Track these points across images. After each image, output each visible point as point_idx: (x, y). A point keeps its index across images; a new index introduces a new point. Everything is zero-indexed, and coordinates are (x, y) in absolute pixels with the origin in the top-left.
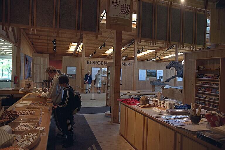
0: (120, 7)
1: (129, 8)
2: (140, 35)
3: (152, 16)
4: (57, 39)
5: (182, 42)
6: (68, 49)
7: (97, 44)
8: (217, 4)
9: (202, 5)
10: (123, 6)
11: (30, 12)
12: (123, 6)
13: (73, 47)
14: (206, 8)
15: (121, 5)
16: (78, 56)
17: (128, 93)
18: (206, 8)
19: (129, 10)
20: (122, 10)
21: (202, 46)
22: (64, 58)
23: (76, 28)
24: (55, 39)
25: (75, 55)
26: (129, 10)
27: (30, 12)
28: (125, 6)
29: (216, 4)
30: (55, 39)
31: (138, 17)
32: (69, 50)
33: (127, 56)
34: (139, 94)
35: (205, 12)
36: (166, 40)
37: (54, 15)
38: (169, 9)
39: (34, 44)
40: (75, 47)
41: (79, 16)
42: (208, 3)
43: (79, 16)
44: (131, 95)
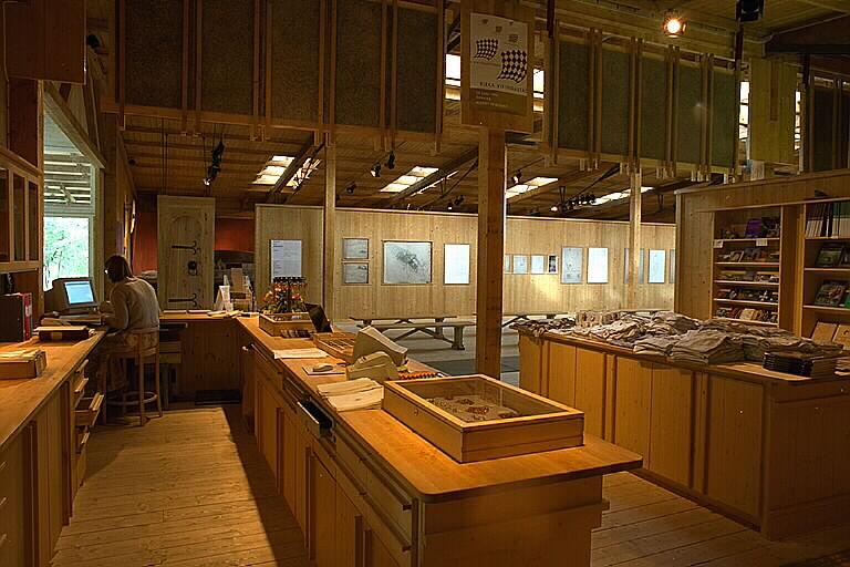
0: (498, 58)
1: (524, 62)
2: (555, 140)
3: (589, 84)
4: (227, 143)
5: (672, 160)
6: (256, 178)
7: (363, 160)
8: (766, 44)
9: (725, 48)
10: (506, 57)
11: (256, 78)
12: (506, 57)
13: (271, 175)
14: (738, 57)
15: (503, 54)
16: (286, 199)
17: (403, 320)
18: (738, 57)
19: (524, 60)
20: (504, 66)
21: (694, 165)
22: (262, 213)
23: (383, 124)
24: (221, 143)
25: (277, 195)
26: (524, 60)
27: (256, 78)
28: (511, 56)
29: (765, 42)
30: (221, 143)
31: (548, 81)
32: (258, 181)
33: (462, 199)
34: (440, 324)
35: (734, 65)
36: (586, 149)
37: (321, 85)
38: (634, 59)
39: (137, 161)
40: (281, 171)
41: (388, 88)
42: (744, 40)
43: (388, 88)
44: (463, 327)
